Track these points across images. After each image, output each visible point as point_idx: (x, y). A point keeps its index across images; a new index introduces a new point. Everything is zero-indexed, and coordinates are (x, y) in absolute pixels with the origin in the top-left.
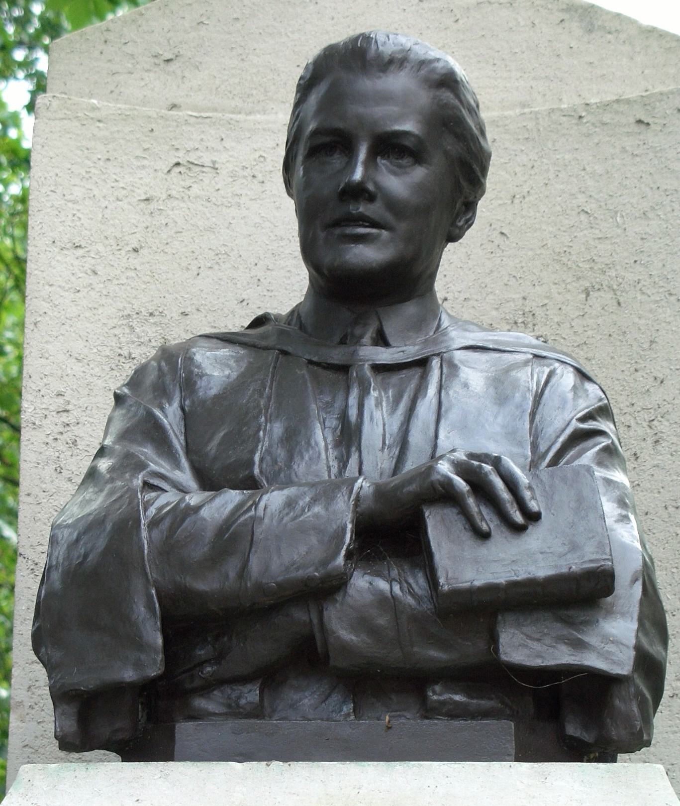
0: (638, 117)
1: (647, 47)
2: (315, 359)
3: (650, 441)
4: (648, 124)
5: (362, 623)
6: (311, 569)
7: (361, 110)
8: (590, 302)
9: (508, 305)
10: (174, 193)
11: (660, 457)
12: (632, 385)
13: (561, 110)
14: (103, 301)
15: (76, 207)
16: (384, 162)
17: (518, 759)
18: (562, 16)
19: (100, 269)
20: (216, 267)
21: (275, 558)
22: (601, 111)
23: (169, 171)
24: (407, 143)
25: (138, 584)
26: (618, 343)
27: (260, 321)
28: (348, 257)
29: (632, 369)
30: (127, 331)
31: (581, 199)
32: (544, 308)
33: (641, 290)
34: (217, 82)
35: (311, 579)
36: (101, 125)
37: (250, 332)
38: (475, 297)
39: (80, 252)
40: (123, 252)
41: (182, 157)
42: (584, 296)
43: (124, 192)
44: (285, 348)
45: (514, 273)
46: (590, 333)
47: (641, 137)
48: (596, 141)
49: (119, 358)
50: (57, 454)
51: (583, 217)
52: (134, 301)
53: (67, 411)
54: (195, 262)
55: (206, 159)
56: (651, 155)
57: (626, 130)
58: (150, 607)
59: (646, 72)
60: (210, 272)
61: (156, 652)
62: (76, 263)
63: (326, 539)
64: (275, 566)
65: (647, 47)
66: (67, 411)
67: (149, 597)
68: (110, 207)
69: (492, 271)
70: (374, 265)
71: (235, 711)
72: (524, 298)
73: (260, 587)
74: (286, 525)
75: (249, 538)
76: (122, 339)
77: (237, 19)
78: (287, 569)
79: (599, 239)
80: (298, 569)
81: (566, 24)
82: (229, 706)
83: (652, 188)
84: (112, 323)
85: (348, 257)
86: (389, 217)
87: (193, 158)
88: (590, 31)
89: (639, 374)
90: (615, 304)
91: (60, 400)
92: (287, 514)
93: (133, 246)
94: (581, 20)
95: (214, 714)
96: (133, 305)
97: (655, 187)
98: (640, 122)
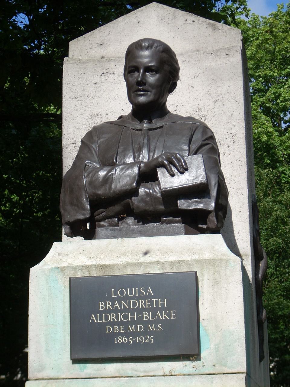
0: (226, 53)
1: (230, 33)
2: (133, 128)
3: (232, 142)
4: (229, 55)
5: (142, 200)
6: (127, 187)
7: (141, 60)
8: (216, 105)
9: (194, 106)
10: (102, 81)
11: (235, 147)
12: (227, 127)
13: (207, 52)
14: (84, 112)
15: (76, 87)
16: (148, 73)
17: (186, 234)
18: (207, 26)
19: (83, 104)
20: (115, 101)
21: (118, 184)
22: (217, 52)
23: (101, 75)
24: (153, 68)
25: (84, 193)
26: (223, 116)
27: (121, 117)
28: (139, 100)
29: (227, 122)
30: (91, 120)
31: (213, 76)
32: (204, 107)
33: (229, 100)
34: (114, 50)
35: (127, 189)
36: (82, 64)
37: (119, 120)
38: (185, 105)
39: (77, 99)
40: (89, 98)
41: (104, 71)
42: (214, 103)
43: (89, 82)
44: (125, 125)
45: (195, 97)
46: (216, 113)
47: (228, 58)
48: (216, 60)
49: (89, 128)
50: (73, 155)
51: (213, 81)
52: (93, 112)
53: (75, 143)
54: (109, 100)
55: (111, 71)
56: (230, 63)
57: (224, 57)
58: (86, 199)
59: (230, 40)
60: (113, 102)
61: (88, 211)
62: (76, 102)
63: (132, 178)
64: (119, 186)
65: (230, 33)
66: (75, 143)
67: (86, 196)
68: (85, 86)
69: (189, 97)
70: (146, 102)
71: (111, 225)
72: (198, 104)
73: (114, 192)
74: (121, 175)
75: (111, 179)
76: (90, 122)
77: (119, 32)
78: (121, 187)
79: (218, 87)
80: (124, 187)
81: (208, 28)
82: (110, 224)
83: (231, 72)
84: (87, 118)
85: (139, 100)
86: (150, 88)
87: (108, 71)
88: (215, 30)
89: (229, 124)
90: (222, 105)
91: (73, 140)
92: (121, 172)
93: (92, 96)
94: (212, 27)
95: (106, 226)
96: (92, 113)
97: (231, 72)
98: (227, 54)
